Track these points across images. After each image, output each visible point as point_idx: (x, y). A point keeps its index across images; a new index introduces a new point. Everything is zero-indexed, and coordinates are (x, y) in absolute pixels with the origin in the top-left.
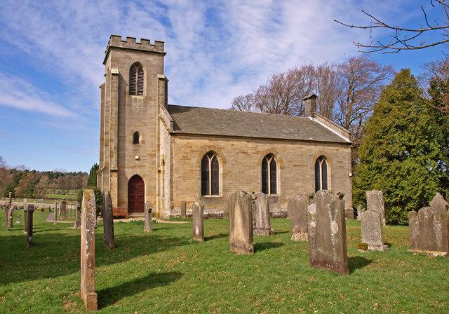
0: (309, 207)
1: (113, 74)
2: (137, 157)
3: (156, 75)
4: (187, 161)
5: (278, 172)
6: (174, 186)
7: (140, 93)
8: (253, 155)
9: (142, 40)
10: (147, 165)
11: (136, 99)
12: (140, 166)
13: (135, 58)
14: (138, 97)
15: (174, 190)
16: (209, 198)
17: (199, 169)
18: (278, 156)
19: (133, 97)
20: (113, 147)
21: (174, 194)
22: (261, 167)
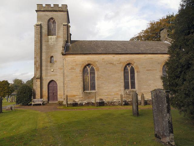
0: (4, 101)
1: (64, 25)
2: (52, 70)
3: (62, 23)
4: (73, 70)
5: (136, 74)
6: (65, 86)
7: (55, 34)
8: (117, 65)
9: (54, 5)
10: (58, 74)
11: (51, 38)
12: (54, 75)
13: (50, 14)
14: (52, 37)
15: (65, 88)
16: (88, 93)
17: (81, 75)
18: (135, 64)
19: (50, 37)
20: (38, 65)
21: (66, 91)
22: (123, 72)
